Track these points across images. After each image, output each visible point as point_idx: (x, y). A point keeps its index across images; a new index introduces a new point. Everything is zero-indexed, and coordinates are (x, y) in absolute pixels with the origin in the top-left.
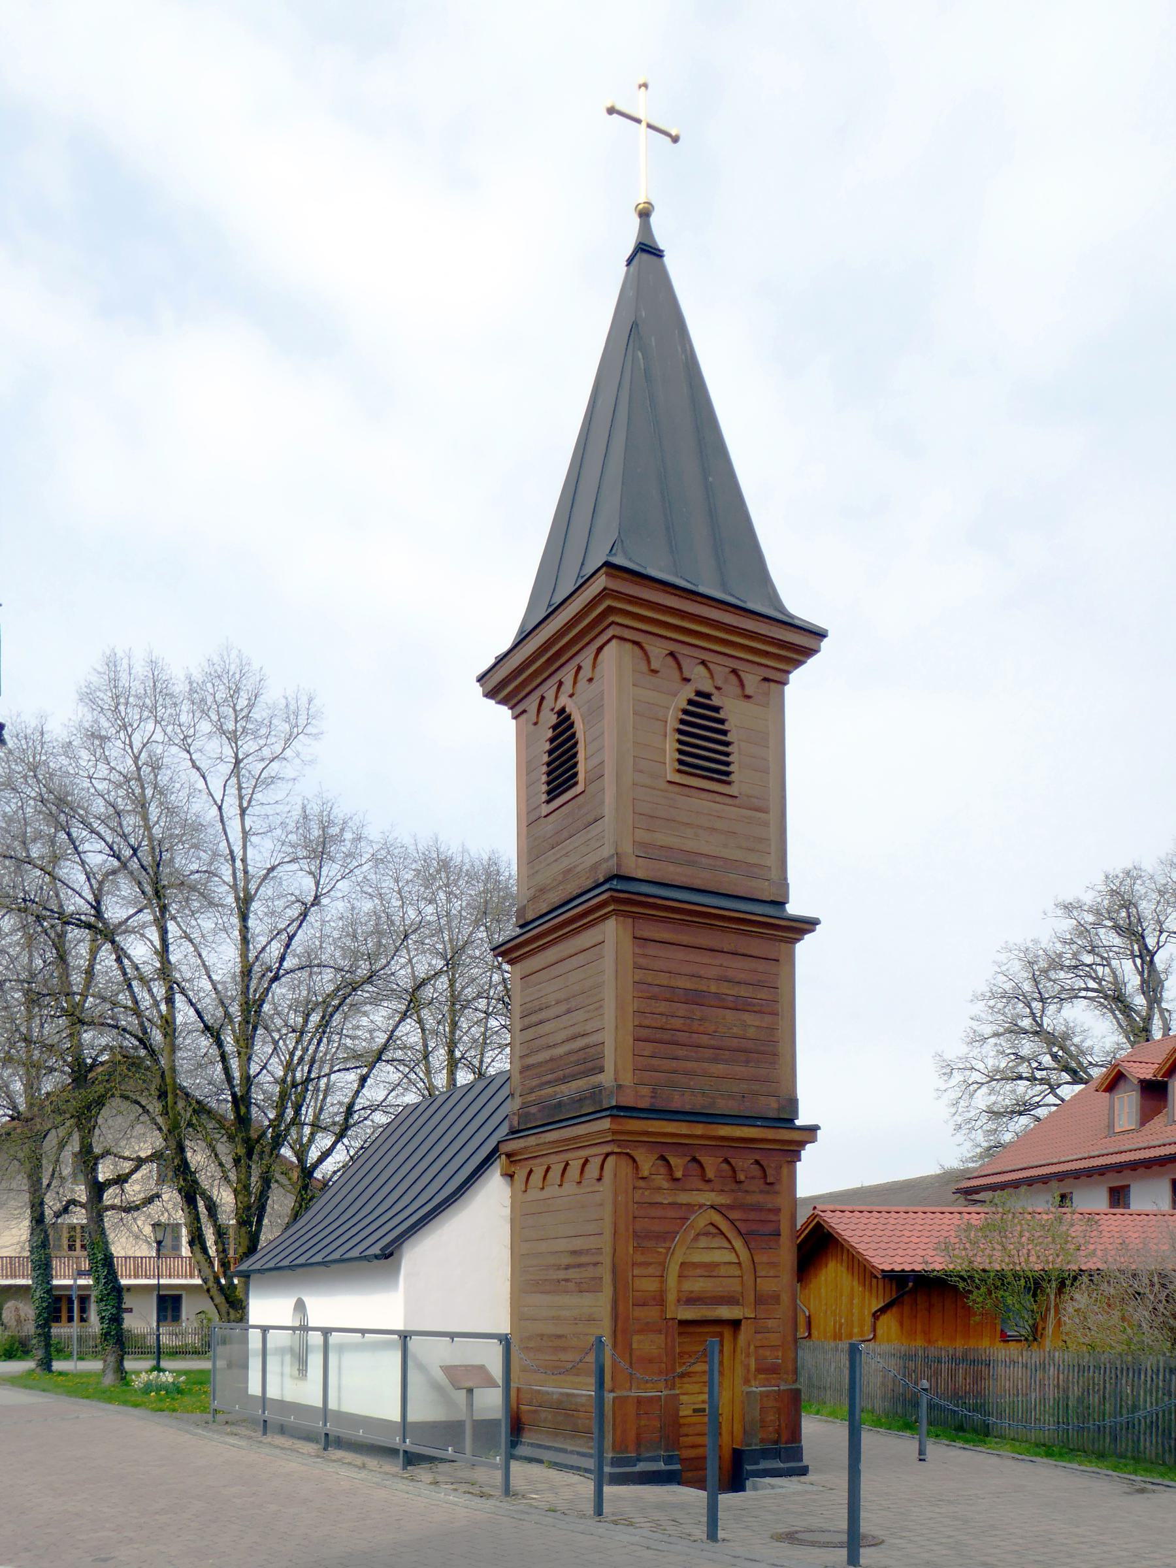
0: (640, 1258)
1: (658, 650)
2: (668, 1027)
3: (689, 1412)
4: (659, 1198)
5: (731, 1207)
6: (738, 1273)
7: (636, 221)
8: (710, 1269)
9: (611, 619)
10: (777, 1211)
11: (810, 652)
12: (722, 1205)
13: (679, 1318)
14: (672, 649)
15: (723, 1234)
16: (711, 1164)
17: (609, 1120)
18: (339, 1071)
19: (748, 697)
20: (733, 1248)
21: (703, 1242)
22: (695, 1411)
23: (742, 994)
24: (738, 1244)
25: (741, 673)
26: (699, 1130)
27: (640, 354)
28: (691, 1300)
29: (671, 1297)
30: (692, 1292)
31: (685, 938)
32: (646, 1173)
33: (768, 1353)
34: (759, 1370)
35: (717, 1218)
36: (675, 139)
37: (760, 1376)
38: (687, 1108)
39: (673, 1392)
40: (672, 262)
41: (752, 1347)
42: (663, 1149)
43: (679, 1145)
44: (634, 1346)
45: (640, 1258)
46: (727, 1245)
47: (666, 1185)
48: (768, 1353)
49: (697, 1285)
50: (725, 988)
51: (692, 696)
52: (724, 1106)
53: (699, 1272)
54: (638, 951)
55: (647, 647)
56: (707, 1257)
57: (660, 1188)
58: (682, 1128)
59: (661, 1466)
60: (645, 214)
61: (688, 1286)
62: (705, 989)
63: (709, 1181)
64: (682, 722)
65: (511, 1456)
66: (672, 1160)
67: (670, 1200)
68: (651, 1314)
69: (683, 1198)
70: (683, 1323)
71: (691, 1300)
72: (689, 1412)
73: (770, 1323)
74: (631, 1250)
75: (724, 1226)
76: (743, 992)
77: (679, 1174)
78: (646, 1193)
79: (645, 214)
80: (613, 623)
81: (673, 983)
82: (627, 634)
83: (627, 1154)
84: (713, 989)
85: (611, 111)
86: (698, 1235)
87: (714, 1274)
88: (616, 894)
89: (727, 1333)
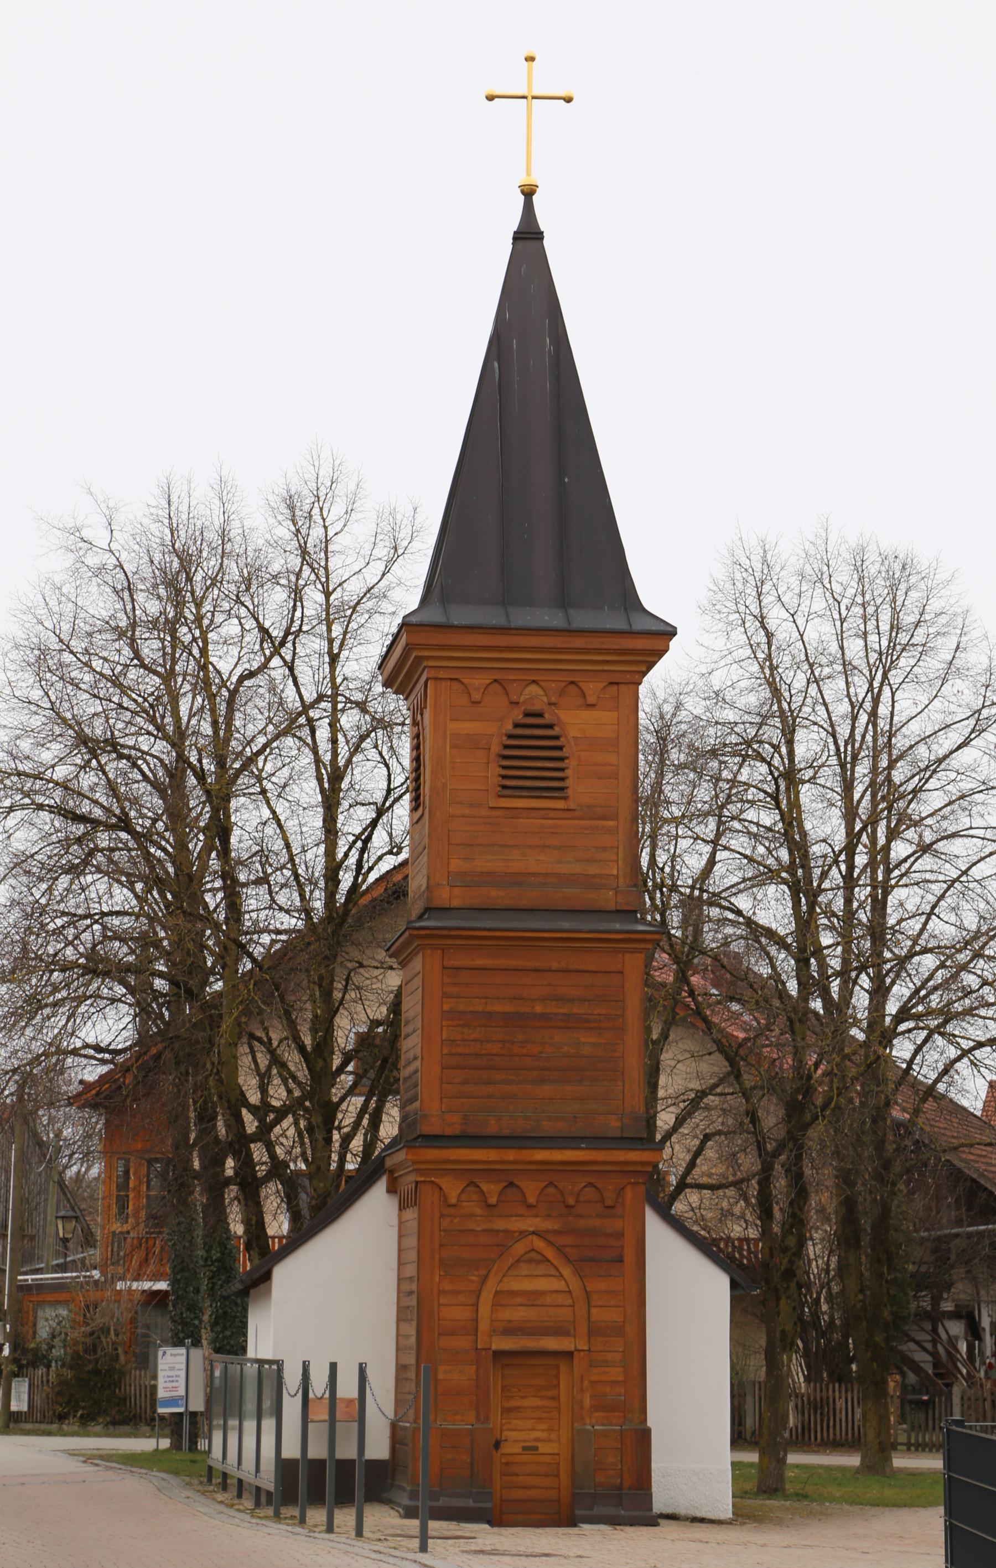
0: (446, 1286)
1: (478, 681)
2: (484, 1052)
3: (518, 1450)
4: (470, 1225)
5: (556, 1232)
6: (570, 1301)
7: (522, 198)
8: (533, 1298)
9: (425, 664)
10: (620, 1235)
11: (660, 653)
12: (548, 1231)
13: (494, 1347)
14: (496, 677)
15: (549, 1261)
16: (531, 1189)
17: (404, 1150)
18: (830, 582)
19: (593, 706)
20: (562, 1276)
21: (524, 1269)
22: (524, 1448)
23: (575, 1011)
24: (567, 1271)
25: (581, 684)
26: (511, 1155)
27: (496, 364)
28: (510, 1330)
29: (484, 1326)
30: (510, 1321)
31: (502, 962)
32: (453, 1201)
33: (608, 1389)
34: (596, 1408)
35: (539, 1244)
36: (569, 100)
37: (597, 1414)
38: (505, 1132)
39: (485, 1426)
40: (549, 244)
41: (586, 1383)
42: (472, 1176)
43: (490, 1172)
44: (441, 1376)
45: (446, 1286)
46: (553, 1272)
47: (479, 1211)
48: (608, 1389)
49: (519, 1314)
50: (553, 1008)
51: (520, 718)
52: (548, 1128)
53: (519, 1300)
54: (447, 980)
55: (465, 681)
56: (528, 1285)
57: (472, 1215)
58: (491, 1155)
59: (470, 1503)
60: (528, 193)
61: (505, 1314)
62: (528, 1010)
63: (530, 1206)
64: (506, 747)
65: (558, 1501)
66: (485, 1187)
67: (485, 1226)
68: (463, 1342)
69: (500, 1225)
70: (498, 1354)
71: (510, 1330)
72: (518, 1450)
73: (610, 1356)
74: (437, 1279)
75: (550, 1253)
76: (576, 1009)
77: (493, 1200)
78: (456, 1221)
79: (528, 193)
80: (425, 667)
81: (490, 1008)
82: (442, 674)
83: (432, 1182)
84: (538, 1009)
85: (490, 98)
86: (517, 1261)
87: (540, 1302)
88: (416, 932)
89: (563, 1368)
